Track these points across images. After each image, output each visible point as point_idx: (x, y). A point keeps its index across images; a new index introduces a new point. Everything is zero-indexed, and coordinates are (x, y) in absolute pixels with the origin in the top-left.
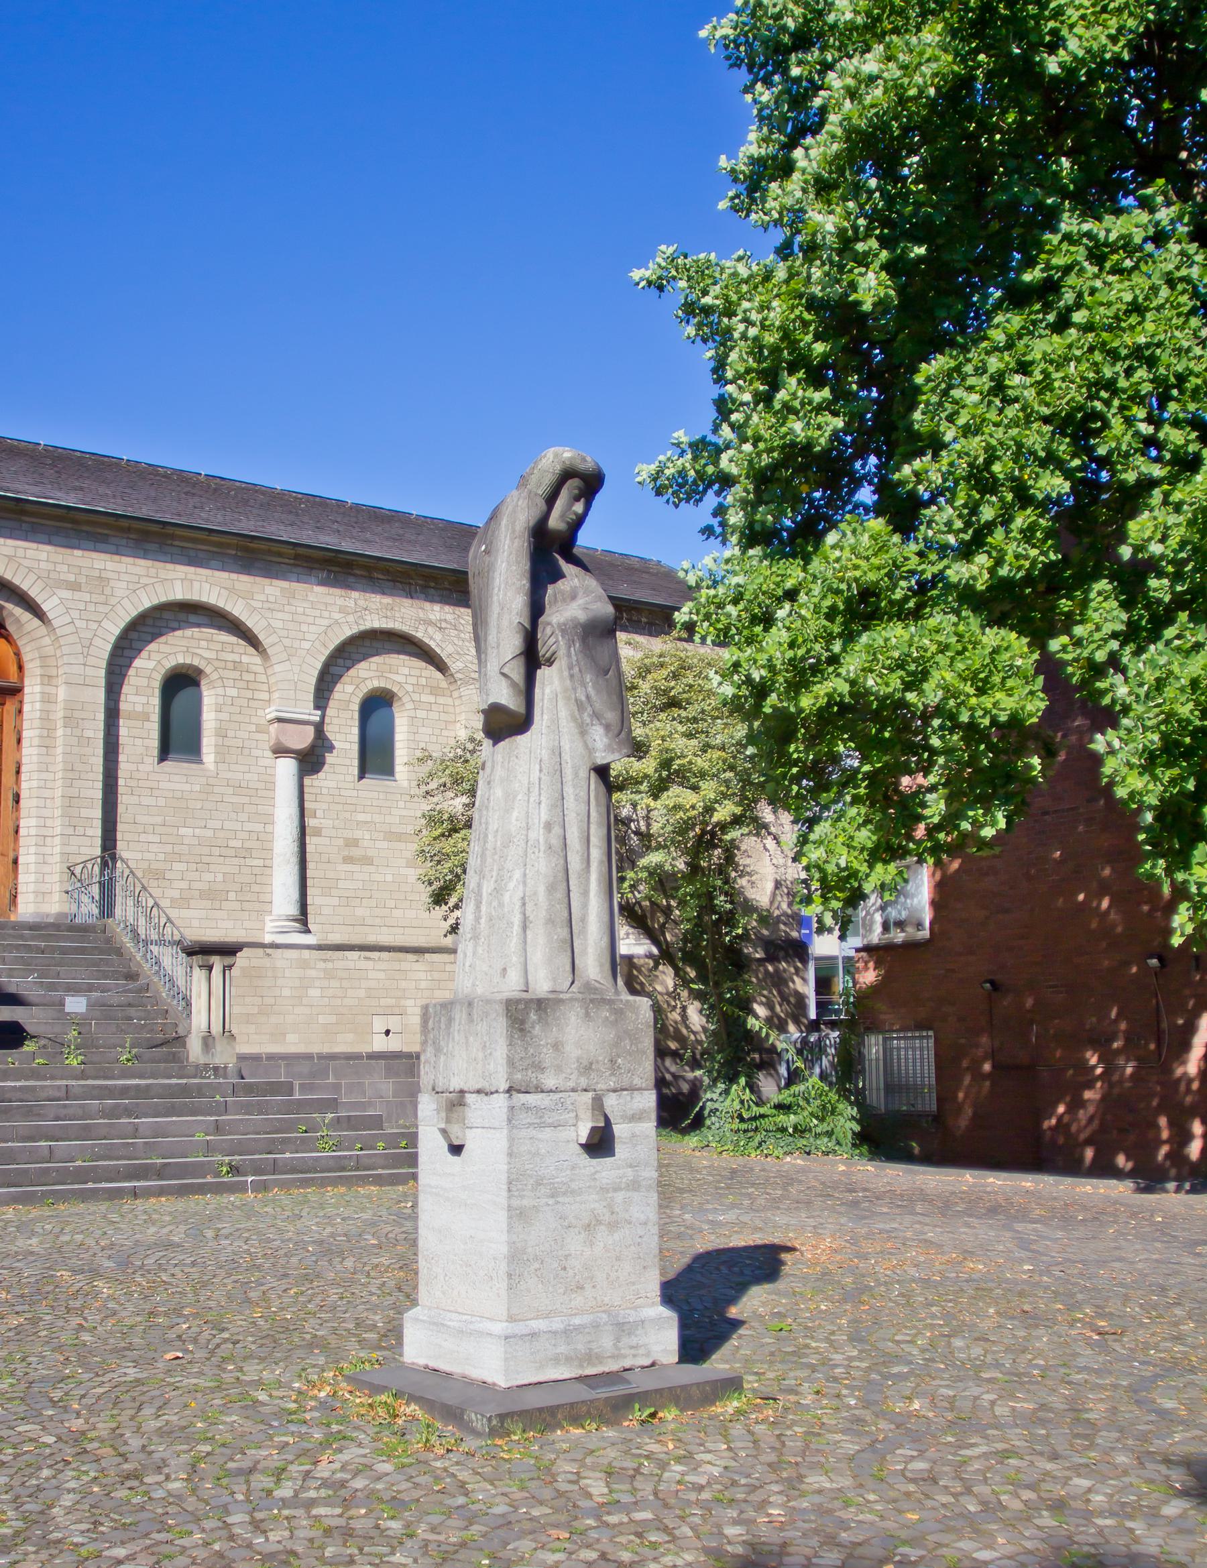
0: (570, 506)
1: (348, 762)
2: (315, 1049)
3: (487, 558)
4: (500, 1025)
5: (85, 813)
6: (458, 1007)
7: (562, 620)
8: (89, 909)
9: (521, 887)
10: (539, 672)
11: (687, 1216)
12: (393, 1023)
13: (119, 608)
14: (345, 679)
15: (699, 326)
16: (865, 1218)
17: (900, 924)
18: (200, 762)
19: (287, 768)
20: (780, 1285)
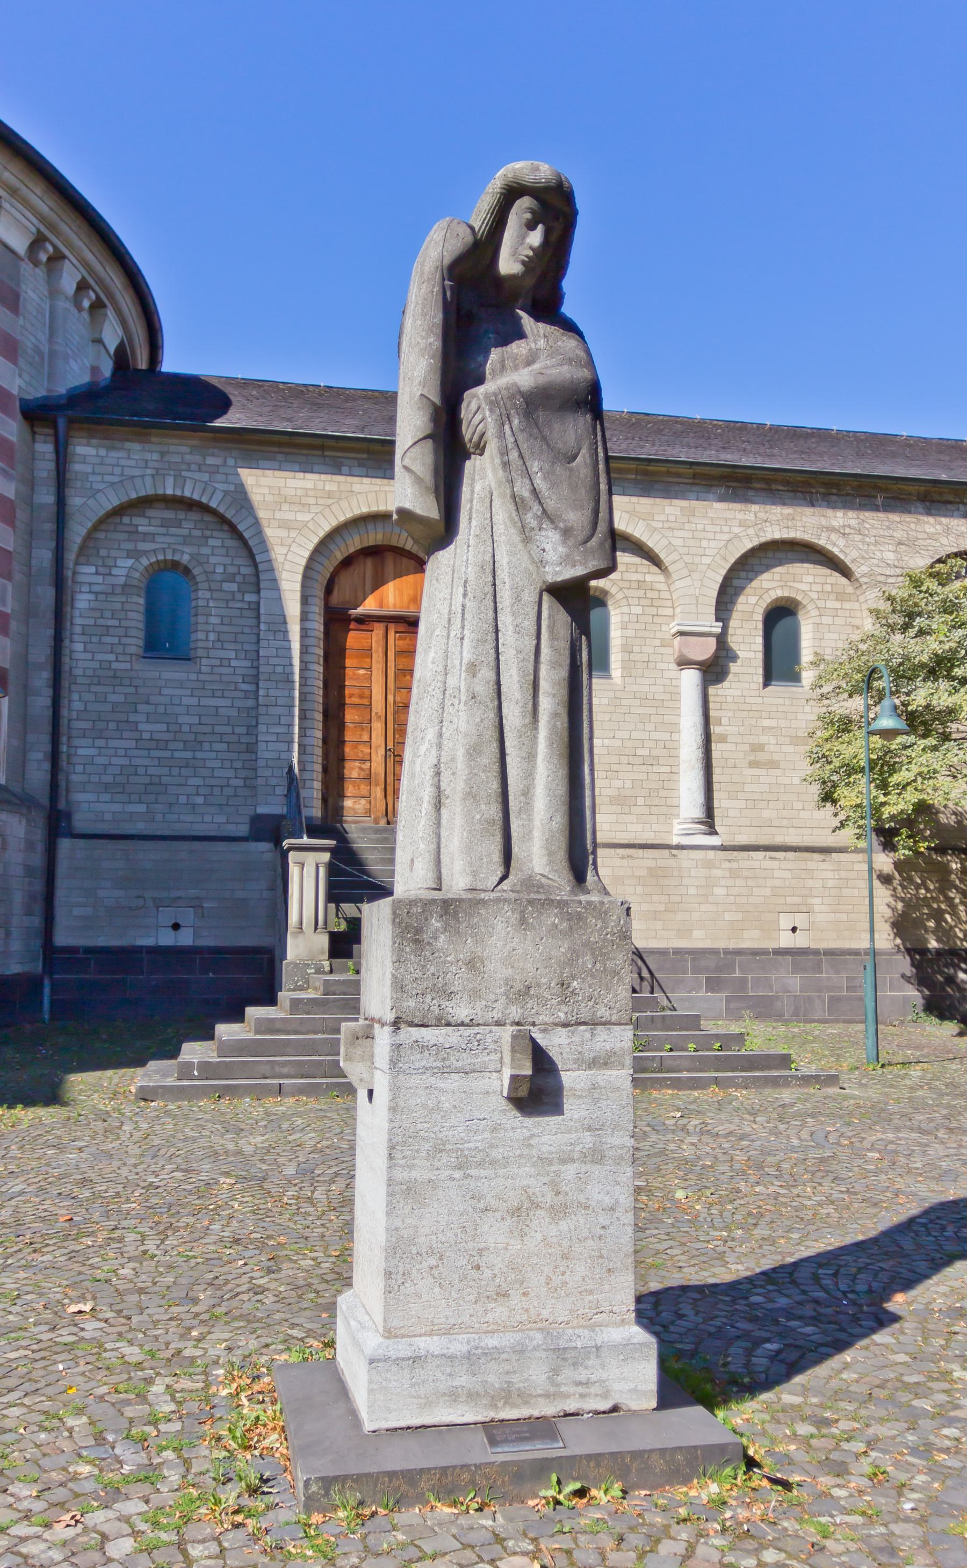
1: (752, 670)
2: (722, 944)
9: (434, 752)
12: (800, 920)
14: (748, 591)
18: (609, 677)
19: (690, 679)
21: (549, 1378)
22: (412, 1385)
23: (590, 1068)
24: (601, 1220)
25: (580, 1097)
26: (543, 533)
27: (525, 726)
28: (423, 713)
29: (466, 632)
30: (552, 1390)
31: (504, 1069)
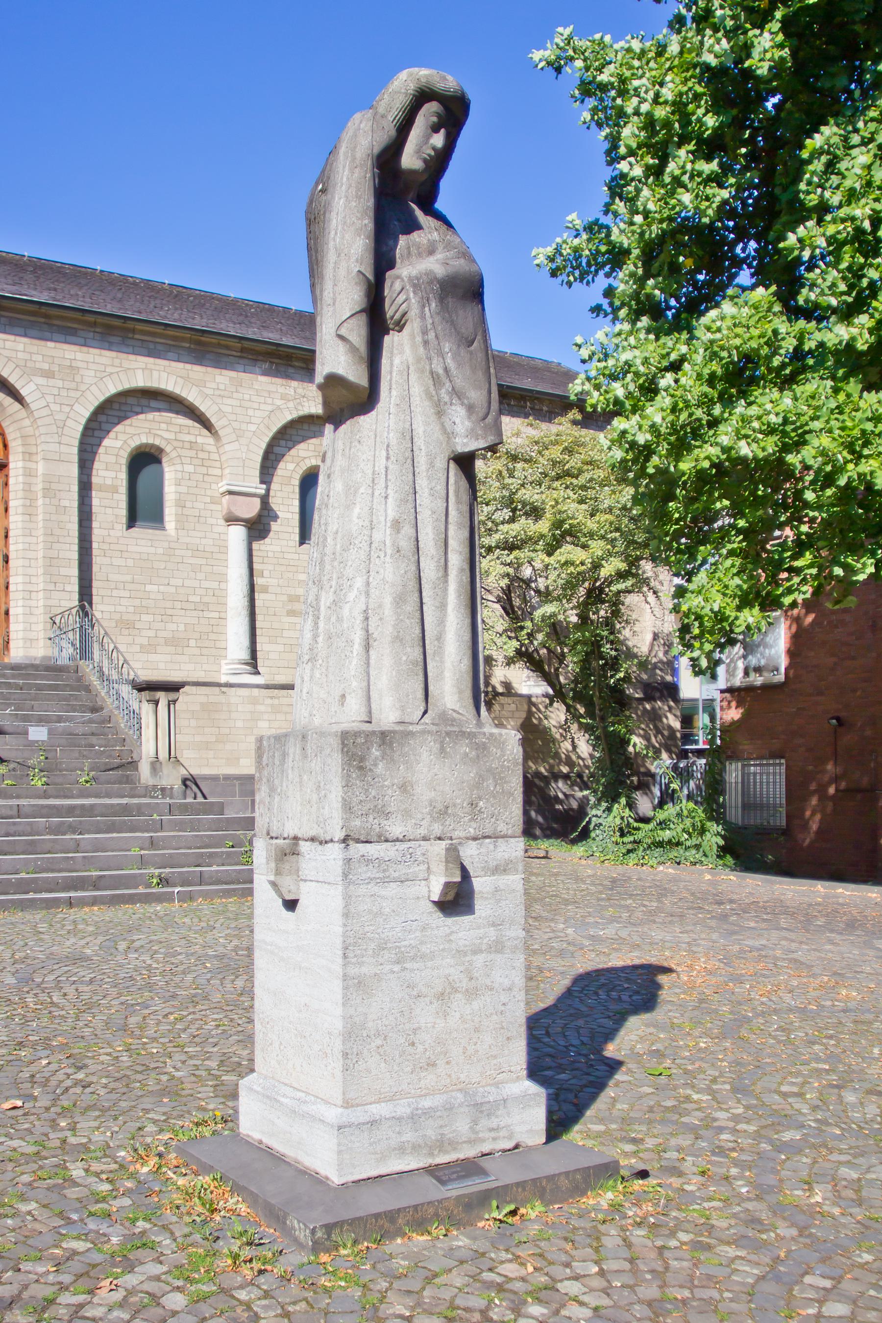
0: (428, 138)
1: (290, 530)
3: (324, 198)
4: (335, 761)
5: (63, 571)
6: (292, 740)
7: (414, 273)
8: (66, 654)
9: (363, 598)
10: (387, 339)
11: (570, 931)
13: (88, 393)
15: (594, 111)
16: (734, 933)
17: (758, 670)
18: (163, 528)
19: (238, 534)
20: (658, 1015)
21: (471, 1128)
22: (371, 1144)
23: (493, 874)
24: (502, 998)
25: (486, 898)
26: (453, 407)
27: (438, 579)
28: (349, 563)
29: (389, 491)
30: (473, 1136)
31: (432, 877)
